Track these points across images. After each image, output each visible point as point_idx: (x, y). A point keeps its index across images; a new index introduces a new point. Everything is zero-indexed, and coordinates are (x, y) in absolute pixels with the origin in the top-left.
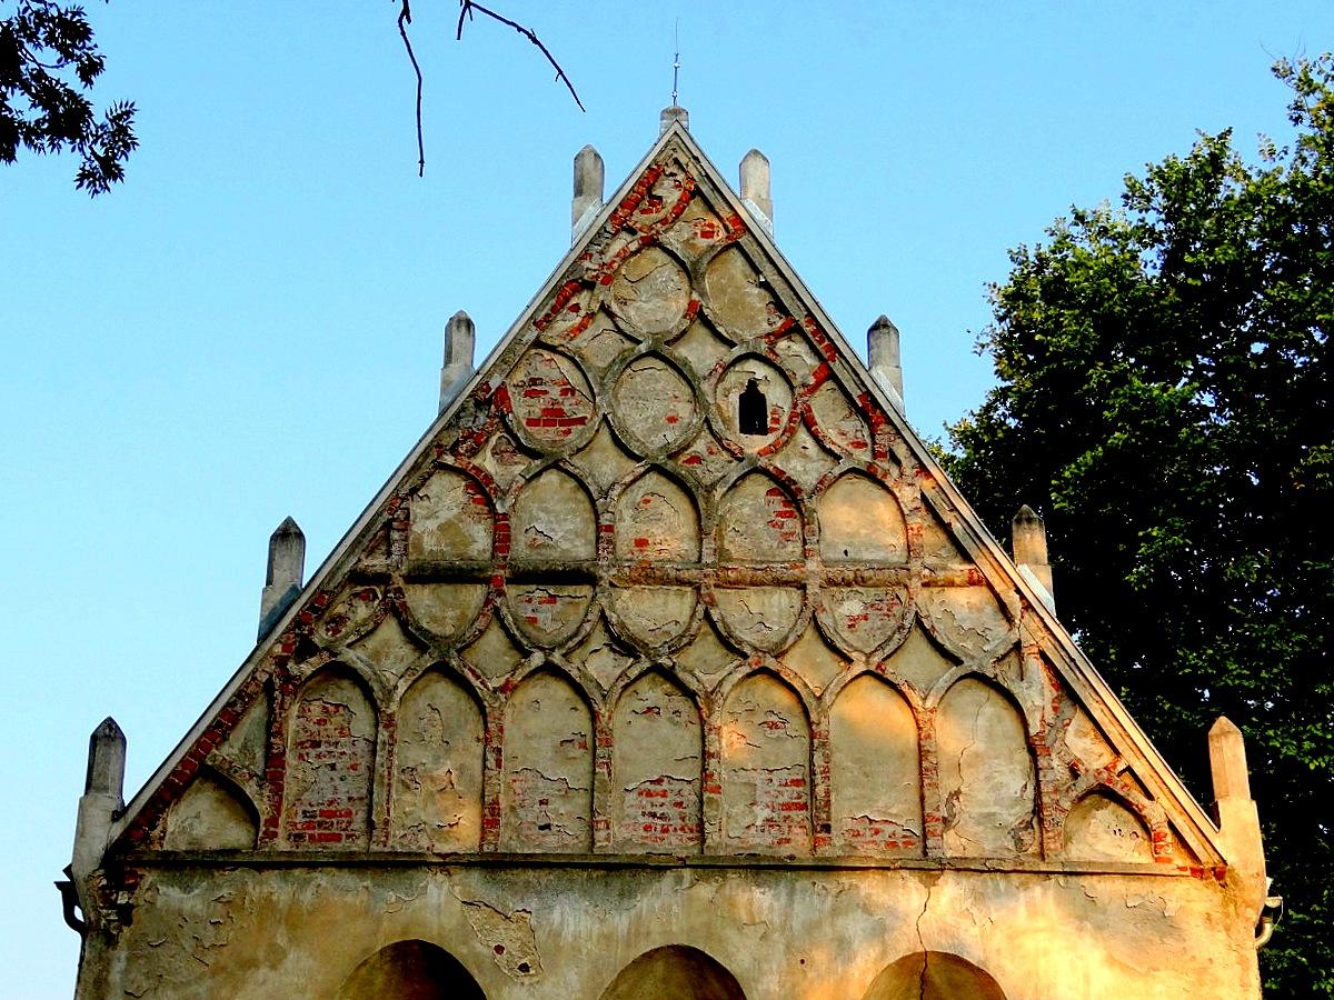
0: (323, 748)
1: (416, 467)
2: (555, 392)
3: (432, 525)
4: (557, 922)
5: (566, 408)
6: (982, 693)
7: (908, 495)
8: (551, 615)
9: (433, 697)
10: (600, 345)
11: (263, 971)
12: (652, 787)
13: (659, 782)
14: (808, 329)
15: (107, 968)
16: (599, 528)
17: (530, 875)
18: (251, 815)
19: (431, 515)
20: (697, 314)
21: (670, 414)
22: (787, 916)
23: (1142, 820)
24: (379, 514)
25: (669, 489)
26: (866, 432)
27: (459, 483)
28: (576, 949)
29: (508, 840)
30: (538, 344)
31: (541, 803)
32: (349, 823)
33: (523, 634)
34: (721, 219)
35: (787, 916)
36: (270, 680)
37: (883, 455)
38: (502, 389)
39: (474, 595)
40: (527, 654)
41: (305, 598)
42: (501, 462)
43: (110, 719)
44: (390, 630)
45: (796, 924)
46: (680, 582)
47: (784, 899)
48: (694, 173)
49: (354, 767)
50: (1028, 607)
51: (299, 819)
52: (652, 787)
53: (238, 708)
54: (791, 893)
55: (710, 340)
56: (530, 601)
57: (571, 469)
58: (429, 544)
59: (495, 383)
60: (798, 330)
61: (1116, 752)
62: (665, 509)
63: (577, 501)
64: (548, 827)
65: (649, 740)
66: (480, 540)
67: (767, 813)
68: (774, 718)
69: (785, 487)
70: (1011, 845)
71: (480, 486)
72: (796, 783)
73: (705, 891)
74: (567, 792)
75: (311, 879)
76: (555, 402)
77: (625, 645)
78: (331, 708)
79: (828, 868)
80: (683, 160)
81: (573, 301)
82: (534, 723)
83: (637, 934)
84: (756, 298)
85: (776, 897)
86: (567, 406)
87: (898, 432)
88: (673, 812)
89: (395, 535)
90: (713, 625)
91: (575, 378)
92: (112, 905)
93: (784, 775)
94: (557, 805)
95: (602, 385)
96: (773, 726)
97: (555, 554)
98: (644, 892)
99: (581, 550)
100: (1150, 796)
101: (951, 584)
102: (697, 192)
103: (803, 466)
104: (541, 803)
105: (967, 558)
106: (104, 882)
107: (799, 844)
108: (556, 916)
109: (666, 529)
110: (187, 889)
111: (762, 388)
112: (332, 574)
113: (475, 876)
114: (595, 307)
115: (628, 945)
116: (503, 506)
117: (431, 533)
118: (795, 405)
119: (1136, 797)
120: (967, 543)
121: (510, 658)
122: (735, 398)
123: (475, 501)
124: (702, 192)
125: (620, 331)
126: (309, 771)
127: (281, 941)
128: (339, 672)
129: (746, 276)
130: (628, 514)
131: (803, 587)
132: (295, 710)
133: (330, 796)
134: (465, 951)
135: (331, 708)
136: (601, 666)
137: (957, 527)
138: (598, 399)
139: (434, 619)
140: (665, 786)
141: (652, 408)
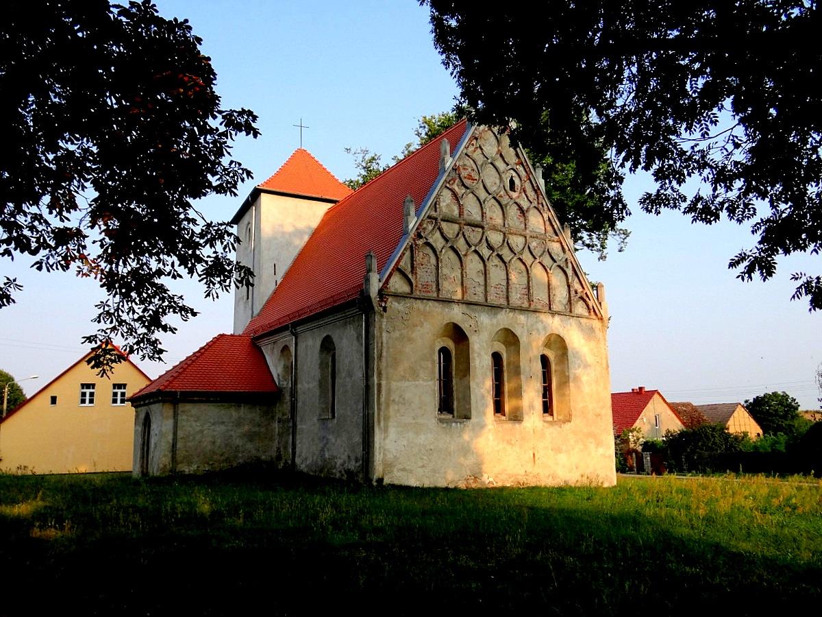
2: (470, 170)
3: (444, 204)
6: (560, 270)
7: (545, 216)
8: (474, 235)
11: (419, 328)
14: (525, 164)
15: (381, 325)
17: (476, 307)
18: (410, 284)
19: (444, 201)
22: (527, 322)
23: (588, 306)
25: (496, 204)
26: (536, 196)
27: (450, 193)
28: (486, 327)
29: (469, 298)
35: (527, 322)
39: (456, 227)
40: (470, 246)
43: (615, 397)
44: (438, 234)
45: (529, 324)
46: (500, 231)
50: (569, 250)
55: (502, 162)
58: (444, 210)
60: (522, 164)
61: (583, 288)
66: (456, 212)
73: (511, 315)
79: (535, 311)
86: (473, 174)
92: (381, 306)
97: (473, 218)
101: (553, 241)
103: (525, 204)
105: (557, 235)
107: (526, 305)
109: (494, 215)
113: (464, 306)
119: (587, 300)
120: (558, 231)
121: (466, 246)
125: (483, 154)
128: (428, 244)
131: (526, 237)
136: (485, 252)
137: (555, 226)
140: (499, 286)
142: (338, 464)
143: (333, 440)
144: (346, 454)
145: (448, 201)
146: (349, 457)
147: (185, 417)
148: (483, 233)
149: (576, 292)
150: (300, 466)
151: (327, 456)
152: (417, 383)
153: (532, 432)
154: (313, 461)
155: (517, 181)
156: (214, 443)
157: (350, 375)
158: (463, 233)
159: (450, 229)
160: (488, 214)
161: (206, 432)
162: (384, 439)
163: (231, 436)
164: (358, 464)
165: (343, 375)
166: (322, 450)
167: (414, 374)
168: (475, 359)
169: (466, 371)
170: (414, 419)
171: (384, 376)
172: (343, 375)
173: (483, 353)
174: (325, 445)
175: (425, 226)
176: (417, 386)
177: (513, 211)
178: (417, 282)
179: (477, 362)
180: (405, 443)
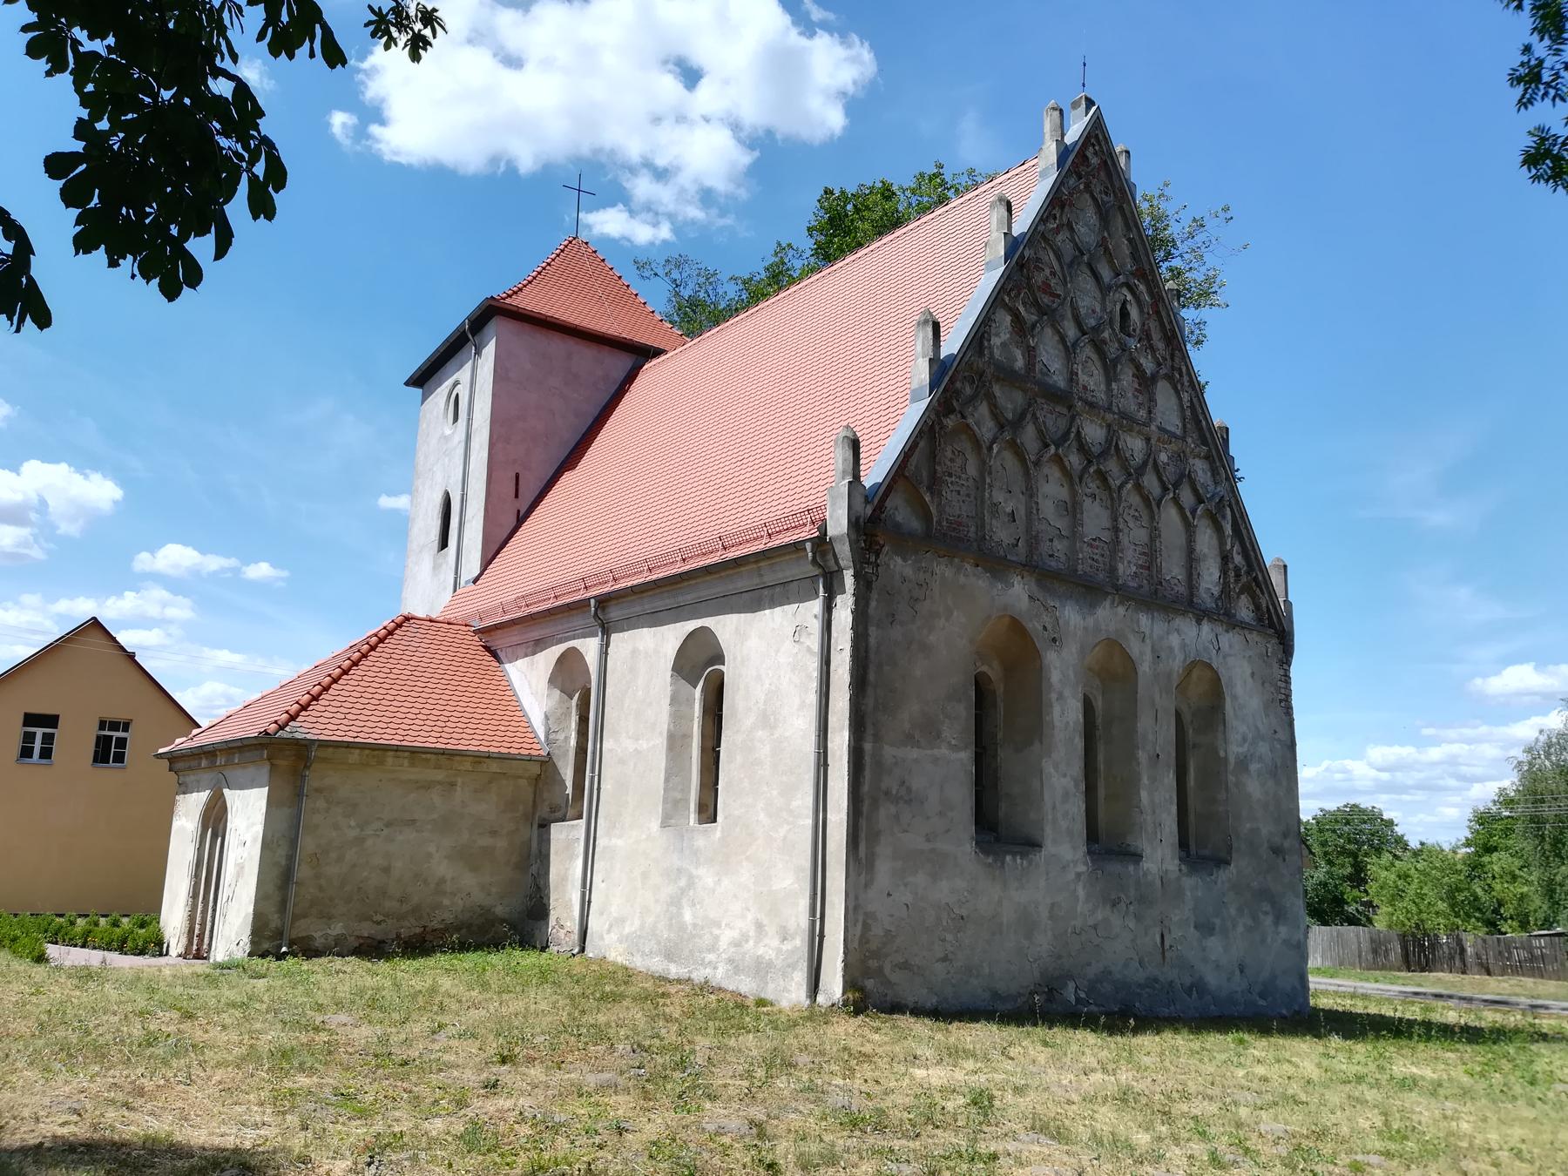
2: (1047, 271)
19: (997, 335)
40: (1046, 446)
44: (984, 409)
66: (1020, 363)
69: (1139, 372)
74: (1061, 536)
84: (1126, 249)
86: (1053, 282)
99: (1060, 381)
103: (1148, 365)
109: (1092, 379)
114: (1065, 220)
122: (1118, 307)
142: (723, 943)
143: (709, 881)
144: (750, 916)
145: (1005, 336)
146: (759, 926)
147: (321, 804)
148: (1073, 418)
149: (1238, 575)
150: (602, 938)
151: (688, 916)
152: (936, 751)
153: (1158, 882)
154: (642, 927)
155: (1134, 313)
156: (387, 870)
157: (767, 720)
158: (1034, 415)
159: (1010, 400)
160: (1083, 378)
161: (369, 842)
162: (866, 886)
163: (430, 855)
164: (787, 946)
165: (749, 722)
166: (675, 902)
167: (929, 731)
168: (1051, 706)
169: (1034, 728)
170: (928, 840)
171: (870, 730)
172: (749, 722)
173: (1067, 693)
174: (683, 891)
175: (958, 385)
176: (935, 761)
177: (1127, 378)
178: (940, 513)
179: (1056, 710)
180: (908, 898)
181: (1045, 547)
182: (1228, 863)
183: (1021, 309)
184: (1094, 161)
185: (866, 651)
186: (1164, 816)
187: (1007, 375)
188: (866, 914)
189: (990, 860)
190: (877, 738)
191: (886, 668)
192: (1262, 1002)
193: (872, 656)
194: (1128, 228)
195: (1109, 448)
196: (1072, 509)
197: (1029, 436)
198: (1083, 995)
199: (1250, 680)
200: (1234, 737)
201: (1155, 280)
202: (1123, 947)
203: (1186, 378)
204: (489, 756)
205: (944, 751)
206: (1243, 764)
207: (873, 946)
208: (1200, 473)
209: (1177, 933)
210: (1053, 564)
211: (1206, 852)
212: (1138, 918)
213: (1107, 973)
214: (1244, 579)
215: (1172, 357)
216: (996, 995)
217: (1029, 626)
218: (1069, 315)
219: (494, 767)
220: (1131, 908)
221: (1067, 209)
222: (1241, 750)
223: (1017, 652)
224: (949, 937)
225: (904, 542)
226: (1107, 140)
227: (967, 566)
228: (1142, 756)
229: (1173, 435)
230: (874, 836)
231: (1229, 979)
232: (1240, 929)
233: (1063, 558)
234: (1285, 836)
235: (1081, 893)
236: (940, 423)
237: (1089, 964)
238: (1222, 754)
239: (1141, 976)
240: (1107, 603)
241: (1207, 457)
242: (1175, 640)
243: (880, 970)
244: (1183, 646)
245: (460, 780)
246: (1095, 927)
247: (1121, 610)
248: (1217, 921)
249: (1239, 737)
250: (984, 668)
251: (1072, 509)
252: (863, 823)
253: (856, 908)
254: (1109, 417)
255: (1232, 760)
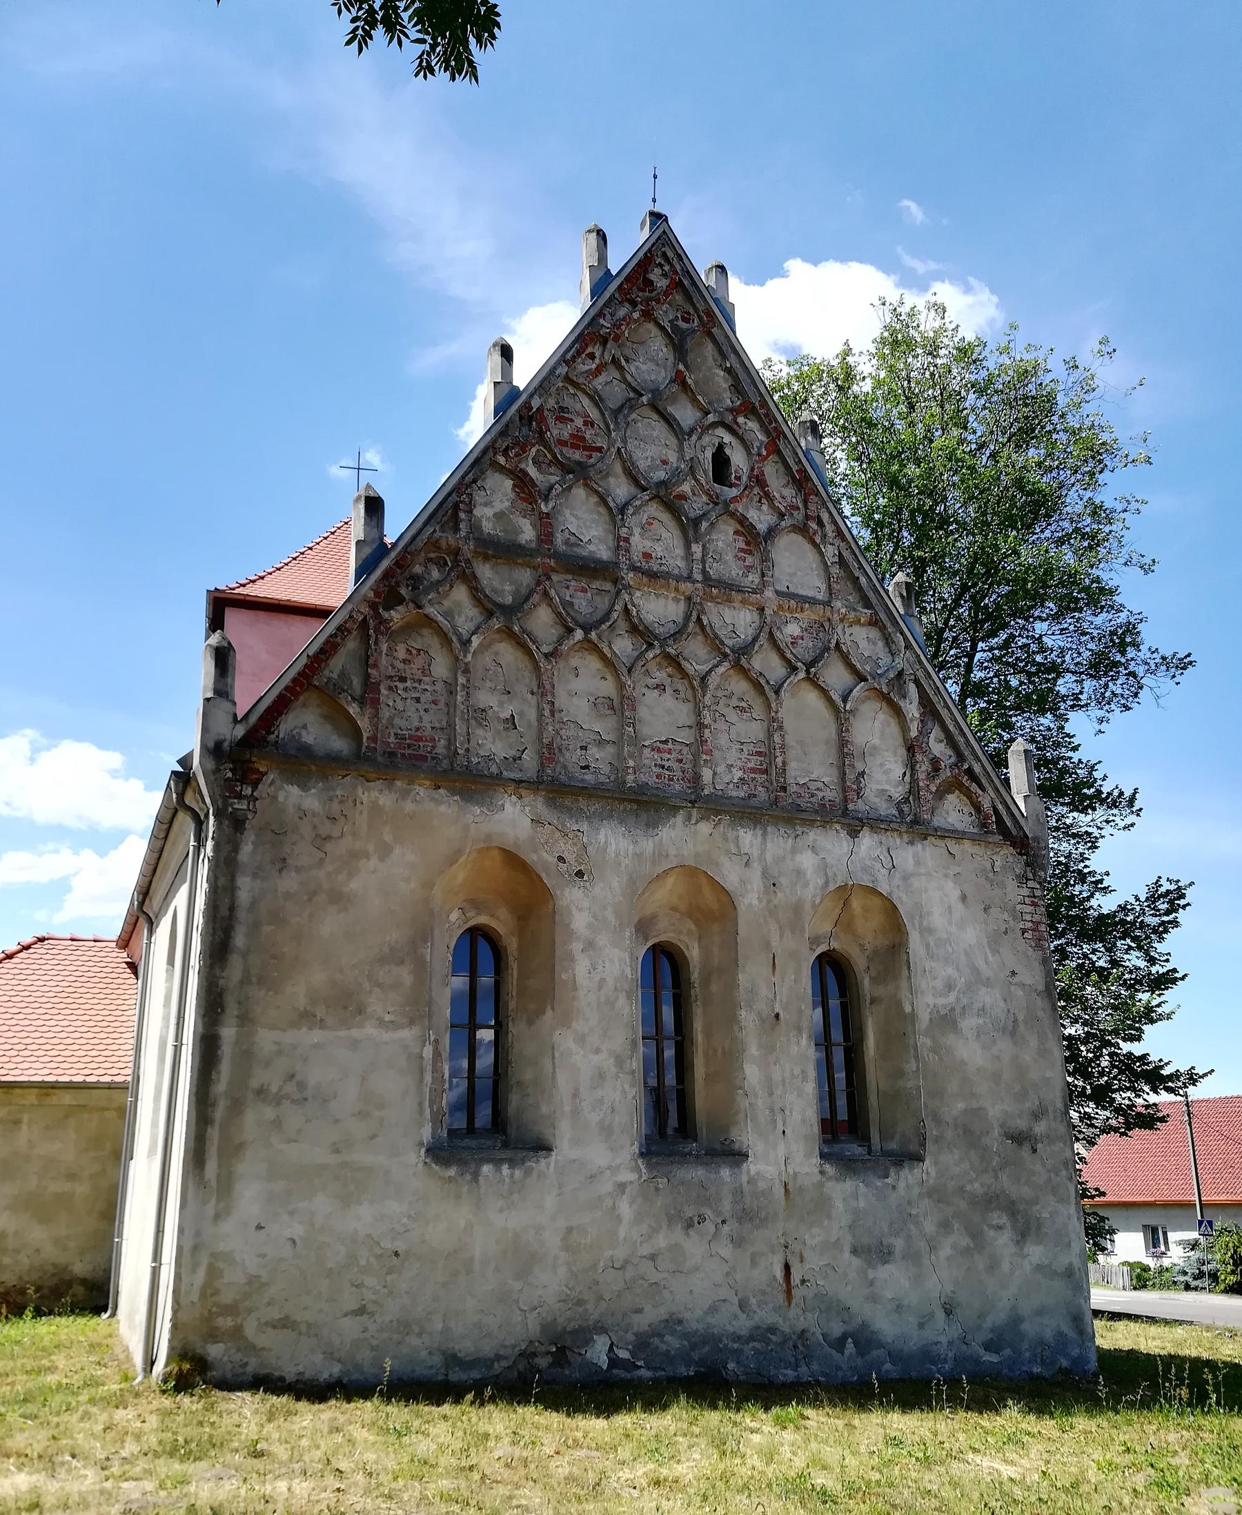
0: (408, 684)
1: (477, 461)
2: (579, 422)
3: (489, 512)
4: (603, 841)
5: (587, 436)
9: (497, 654)
10: (610, 386)
11: (374, 862)
12: (661, 746)
13: (666, 742)
16: (619, 538)
20: (679, 379)
21: (664, 458)
22: (763, 851)
24: (449, 494)
30: (567, 379)
31: (582, 748)
32: (434, 747)
33: (568, 614)
34: (696, 309)
36: (365, 619)
37: (813, 518)
38: (540, 409)
39: (525, 577)
40: (570, 631)
41: (393, 555)
42: (540, 470)
44: (460, 594)
45: (769, 857)
47: (760, 839)
48: (678, 268)
49: (435, 702)
51: (392, 739)
52: (661, 746)
53: (339, 640)
54: (765, 834)
56: (568, 587)
57: (595, 486)
59: (536, 403)
62: (665, 535)
63: (599, 514)
64: (587, 767)
65: (662, 714)
66: (527, 533)
67: (740, 774)
68: (744, 704)
69: (746, 529)
70: (896, 813)
71: (522, 483)
72: (759, 754)
74: (601, 743)
75: (411, 790)
76: (579, 430)
77: (639, 630)
78: (414, 652)
80: (670, 254)
81: (589, 350)
82: (578, 685)
83: (660, 854)
84: (721, 380)
85: (755, 836)
87: (824, 503)
88: (675, 766)
89: (462, 515)
90: (703, 627)
91: (594, 414)
93: (751, 747)
94: (593, 751)
95: (617, 423)
96: (743, 710)
98: (664, 825)
99: (603, 552)
100: (983, 789)
102: (681, 283)
103: (761, 518)
104: (582, 748)
106: (230, 775)
108: (602, 837)
110: (304, 787)
111: (727, 451)
112: (414, 538)
114: (608, 358)
115: (654, 862)
116: (546, 506)
117: (488, 519)
118: (752, 469)
122: (709, 454)
123: (521, 498)
124: (684, 281)
125: (625, 381)
126: (398, 701)
127: (388, 838)
129: (715, 360)
130: (637, 531)
132: (384, 647)
133: (416, 724)
134: (535, 857)
135: (414, 652)
136: (623, 646)
138: (613, 434)
139: (494, 590)
140: (670, 745)
141: (652, 447)
152: (355, 1033)
153: (779, 1192)
158: (546, 594)
162: (217, 1217)
170: (337, 1151)
171: (232, 1010)
173: (602, 940)
176: (354, 1044)
177: (724, 537)
179: (582, 967)
180: (298, 1230)
181: (572, 758)
182: (920, 1159)
183: (532, 471)
184: (662, 283)
185: (232, 908)
186: (791, 1098)
187: (504, 551)
188: (212, 1255)
189: (452, 1172)
190: (245, 1020)
191: (267, 929)
192: (994, 1358)
193: (242, 915)
194: (724, 356)
195: (685, 625)
196: (621, 707)
197: (542, 622)
198: (623, 1354)
199: (959, 908)
200: (922, 983)
201: (769, 414)
202: (705, 1280)
203: (829, 528)
204: (55, 1086)
205: (370, 1030)
206: (947, 1021)
207: (226, 1298)
208: (863, 644)
209: (815, 1261)
210: (589, 777)
211: (893, 1145)
212: (738, 1242)
213: (673, 1323)
214: (946, 774)
215: (805, 502)
216: (453, 1360)
217: (531, 858)
218: (618, 468)
219: (68, 1098)
220: (726, 1229)
221: (610, 344)
222: (942, 1001)
223: (527, 891)
224: (370, 1281)
225: (304, 763)
226: (681, 256)
227: (422, 791)
228: (747, 1017)
229: (812, 601)
230: (233, 1150)
231: (921, 1326)
232: (946, 1251)
233: (606, 769)
234: (1036, 1116)
235: (626, 1209)
236: (377, 616)
237: (639, 1311)
238: (908, 1009)
239: (743, 1324)
240: (680, 818)
241: (874, 622)
242: (807, 861)
243: (237, 1332)
244: (824, 867)
245: (26, 1117)
246: (653, 1257)
247: (705, 828)
248: (899, 1244)
249: (939, 984)
250: (483, 919)
251: (621, 707)
252: (214, 1134)
253: (196, 1249)
254: (687, 587)
255: (924, 1017)
